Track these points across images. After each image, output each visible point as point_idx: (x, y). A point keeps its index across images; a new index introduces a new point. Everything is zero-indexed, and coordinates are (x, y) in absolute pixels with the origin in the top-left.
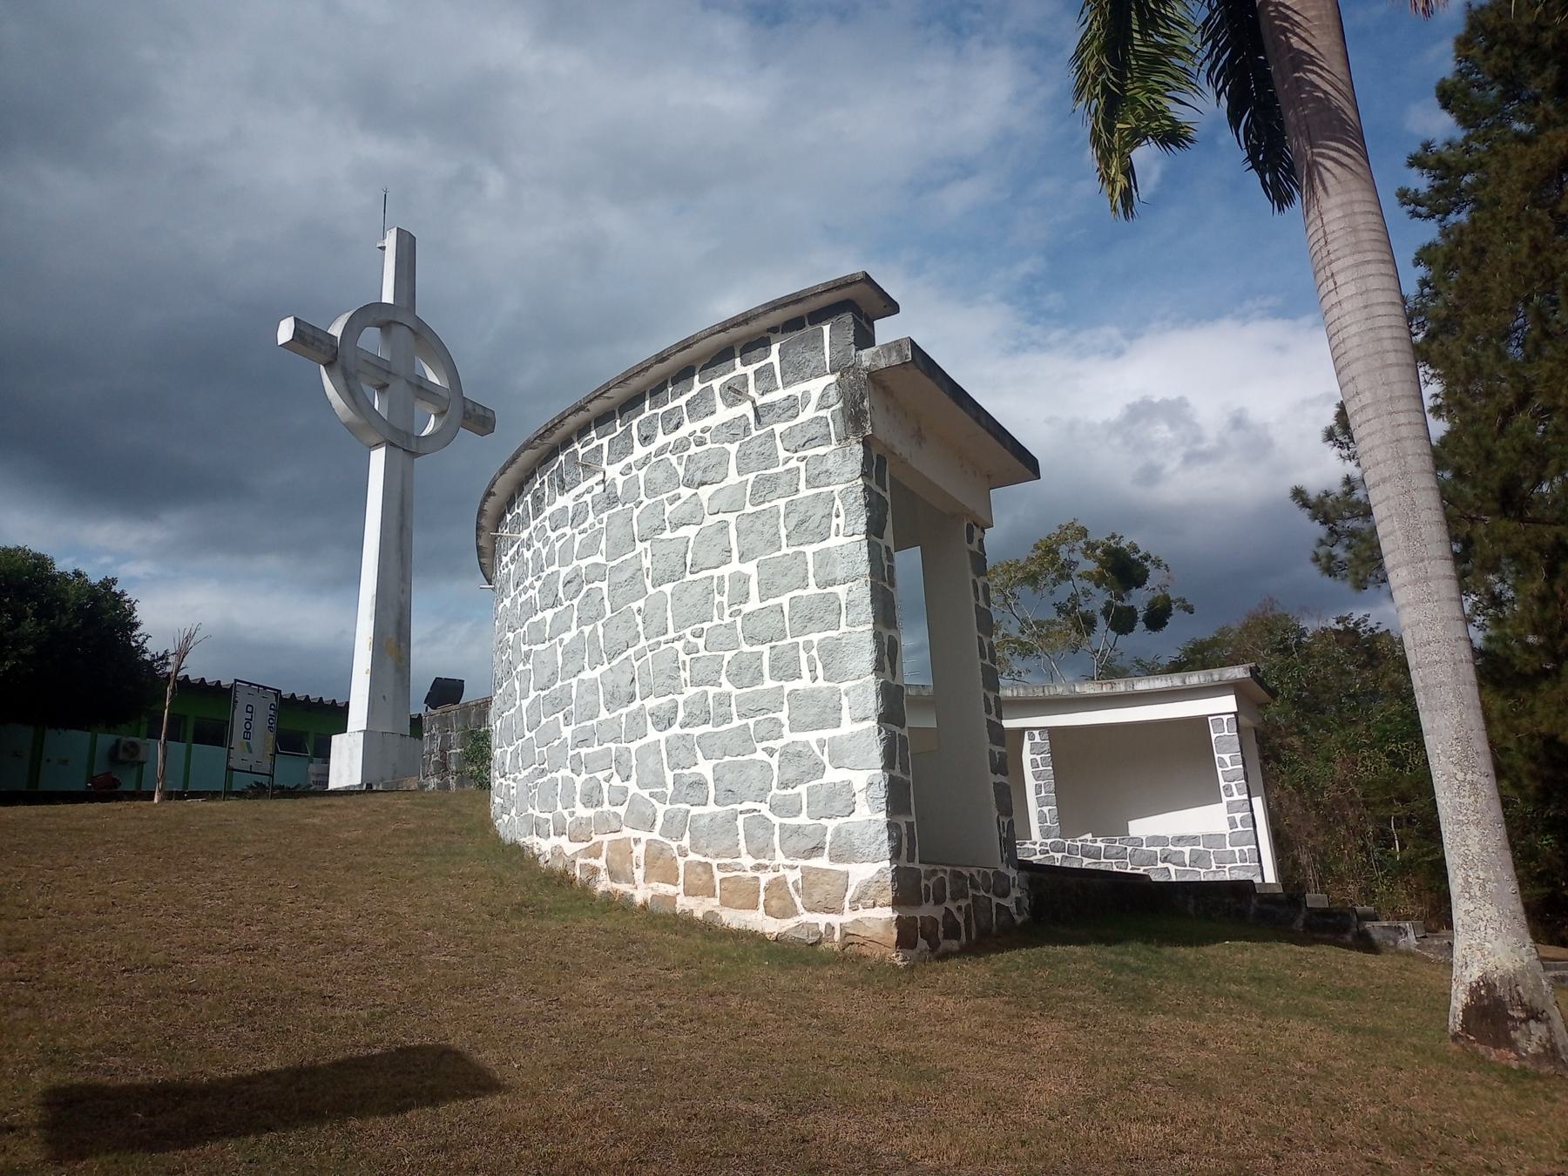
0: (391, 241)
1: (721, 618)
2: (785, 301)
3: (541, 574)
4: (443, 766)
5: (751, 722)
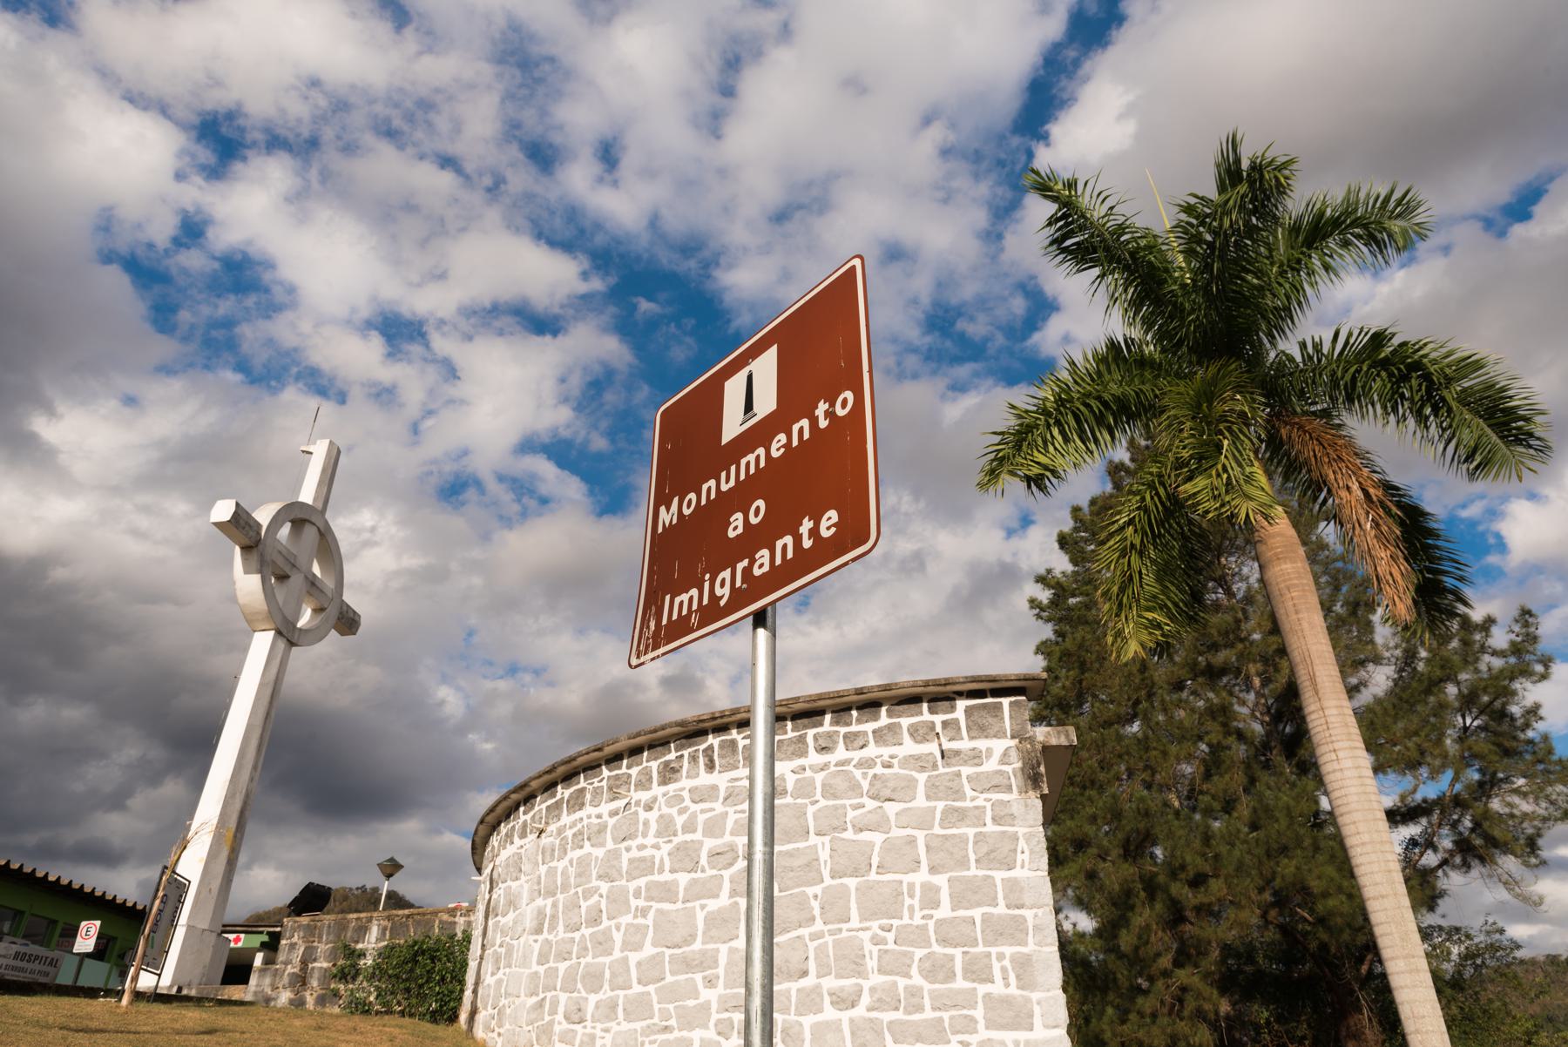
0: (320, 450)
1: (911, 918)
2: (983, 678)
3: (672, 838)
4: (301, 980)
5: (946, 1015)
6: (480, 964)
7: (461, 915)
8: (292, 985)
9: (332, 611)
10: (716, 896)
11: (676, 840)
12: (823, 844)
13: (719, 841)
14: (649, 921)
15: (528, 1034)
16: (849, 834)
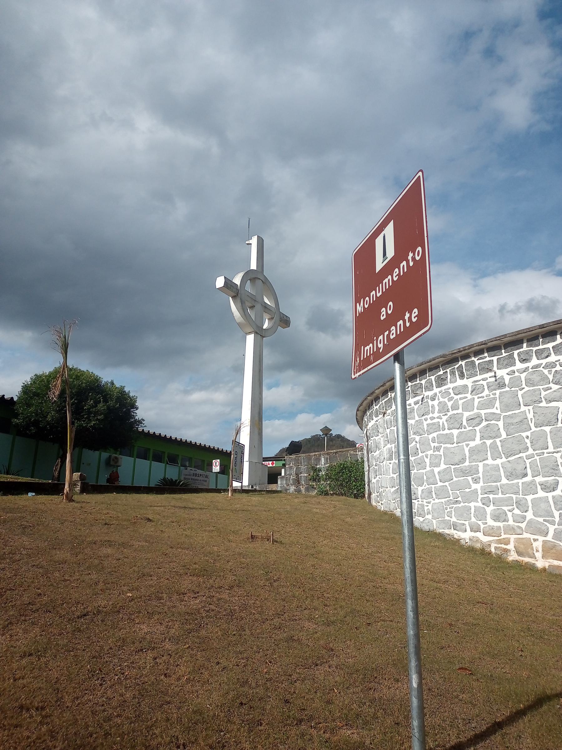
3: (447, 413)
4: (297, 481)
6: (369, 473)
7: (359, 451)
8: (294, 484)
9: (277, 318)
10: (474, 440)
11: (449, 414)
12: (529, 410)
13: (471, 413)
14: (441, 452)
15: (394, 504)
16: (544, 404)
